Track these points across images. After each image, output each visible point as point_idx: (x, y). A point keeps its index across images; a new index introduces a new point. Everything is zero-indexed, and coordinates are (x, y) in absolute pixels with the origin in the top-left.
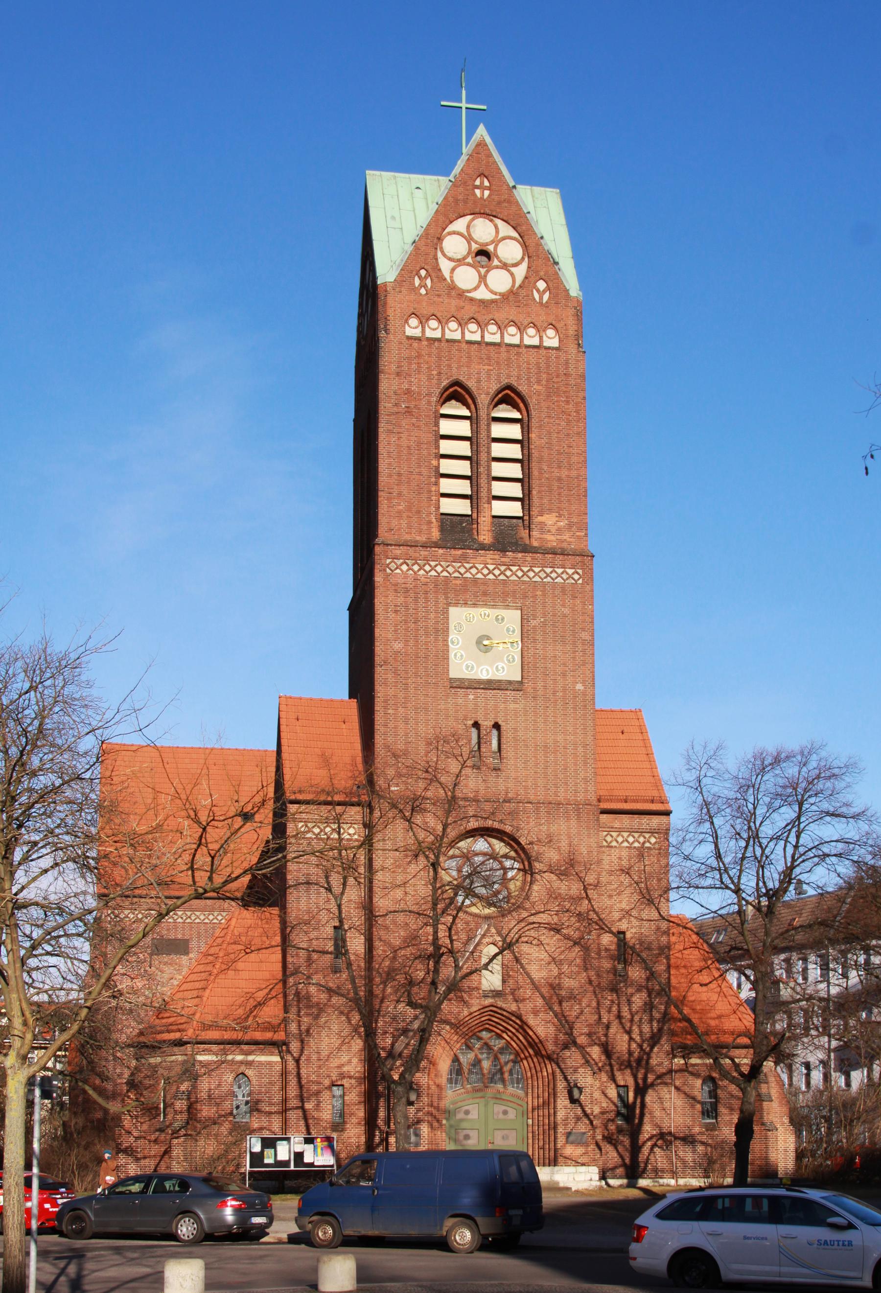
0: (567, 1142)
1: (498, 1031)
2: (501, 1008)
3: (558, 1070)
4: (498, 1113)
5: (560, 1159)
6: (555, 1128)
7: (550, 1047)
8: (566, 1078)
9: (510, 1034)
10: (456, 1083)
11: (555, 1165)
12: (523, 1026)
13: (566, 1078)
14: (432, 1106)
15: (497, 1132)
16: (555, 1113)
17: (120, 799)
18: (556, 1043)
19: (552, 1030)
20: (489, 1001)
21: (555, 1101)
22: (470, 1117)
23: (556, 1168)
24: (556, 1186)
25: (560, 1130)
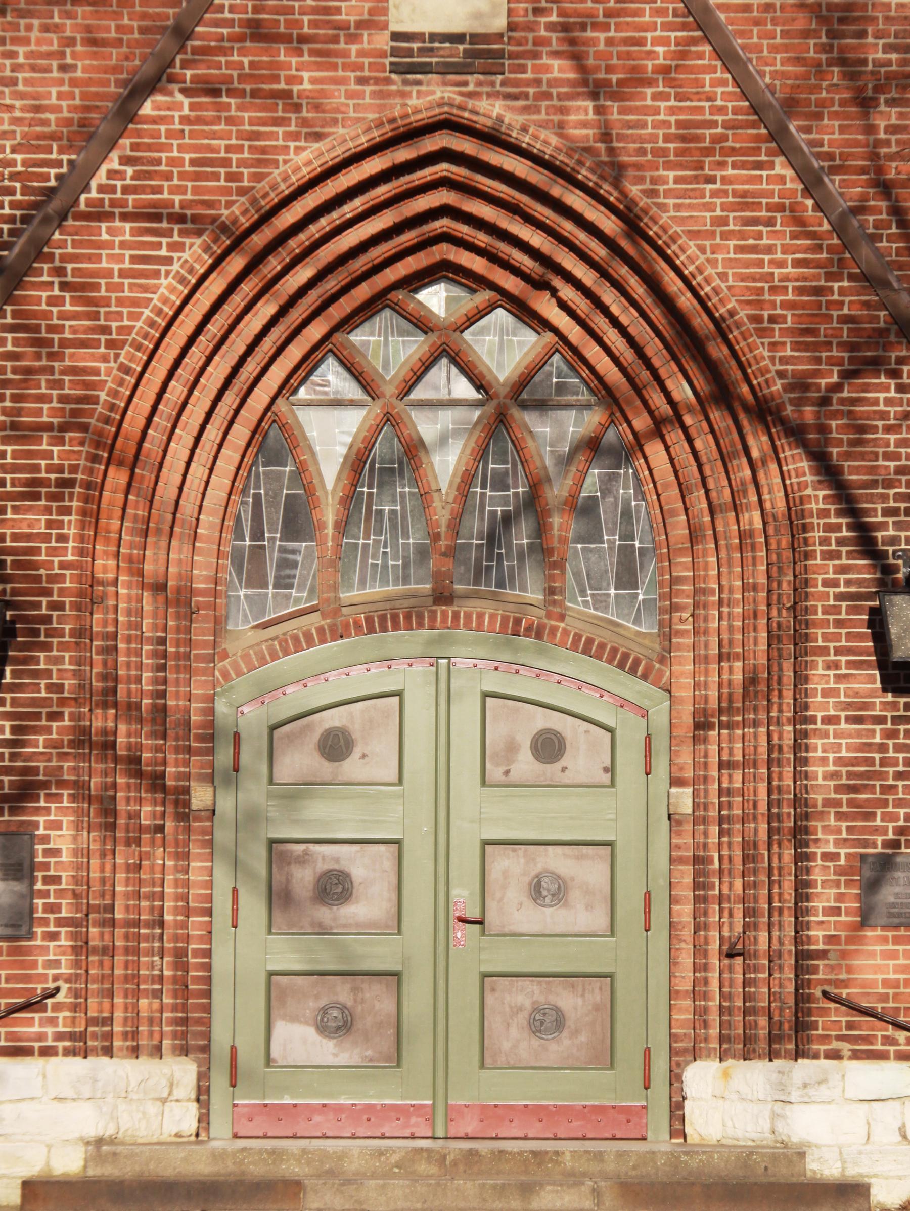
0: (865, 918)
1: (510, 283)
2: (493, 137)
3: (818, 498)
4: (512, 748)
5: (830, 1020)
6: (801, 835)
7: (771, 361)
8: (866, 542)
9: (567, 293)
10: (283, 583)
11: (799, 1054)
12: (637, 243)
13: (866, 542)
14: (108, 698)
15: (503, 863)
16: (800, 745)
17: (604, 158)
18: (807, 336)
19: (783, 259)
20: (428, 97)
21: (800, 678)
22: (352, 767)
23: (805, 1068)
24: (782, 1173)
25: (830, 839)
